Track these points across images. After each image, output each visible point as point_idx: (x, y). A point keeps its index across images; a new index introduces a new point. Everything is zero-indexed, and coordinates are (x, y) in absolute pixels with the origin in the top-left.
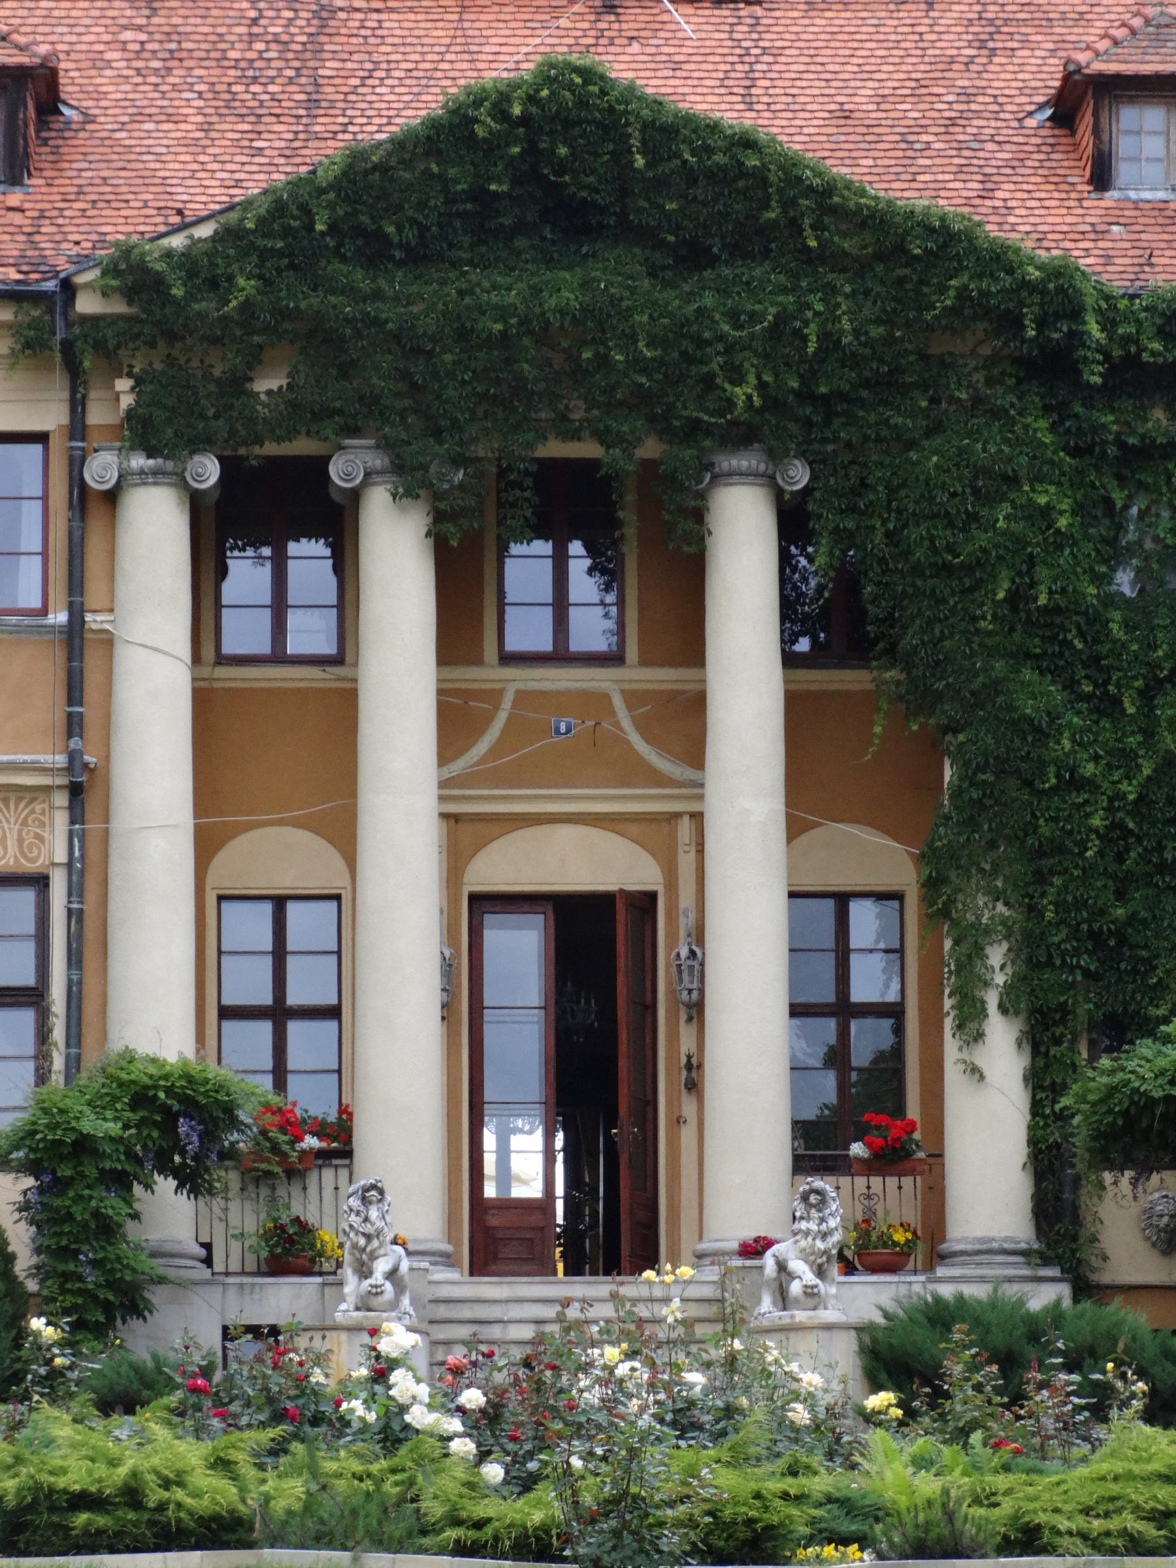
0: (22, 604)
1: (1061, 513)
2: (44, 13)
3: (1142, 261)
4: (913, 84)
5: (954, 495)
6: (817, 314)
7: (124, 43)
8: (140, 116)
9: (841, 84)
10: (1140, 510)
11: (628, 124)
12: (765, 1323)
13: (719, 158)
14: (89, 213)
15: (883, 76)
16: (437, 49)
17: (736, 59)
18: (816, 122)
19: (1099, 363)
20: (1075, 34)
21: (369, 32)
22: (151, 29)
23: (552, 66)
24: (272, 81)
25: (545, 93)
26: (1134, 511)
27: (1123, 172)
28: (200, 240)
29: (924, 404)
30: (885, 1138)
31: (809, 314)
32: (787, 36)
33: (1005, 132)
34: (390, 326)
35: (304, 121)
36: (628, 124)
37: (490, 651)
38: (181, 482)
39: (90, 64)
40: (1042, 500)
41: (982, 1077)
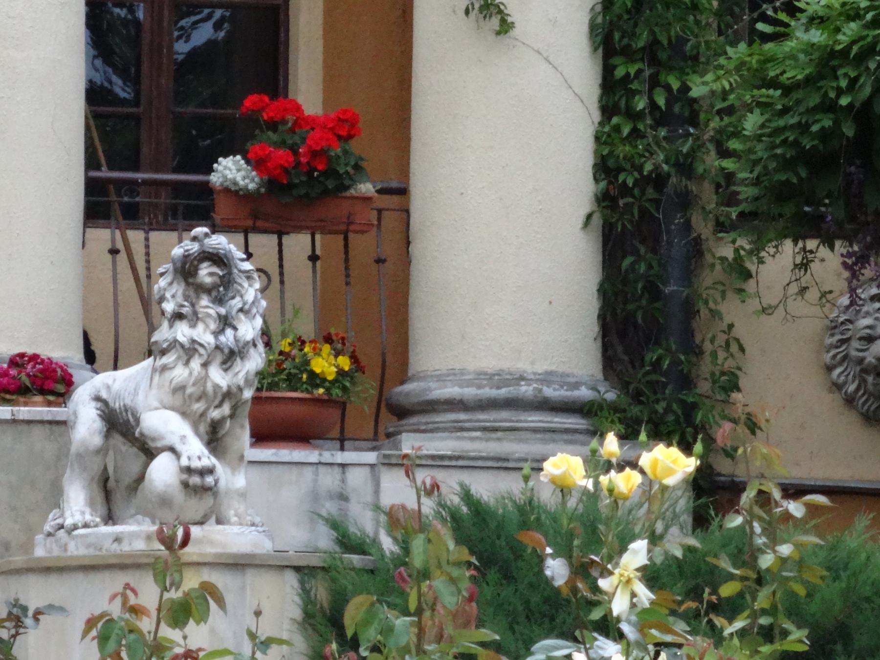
12: (76, 550)
30: (294, 149)
41: (505, 27)
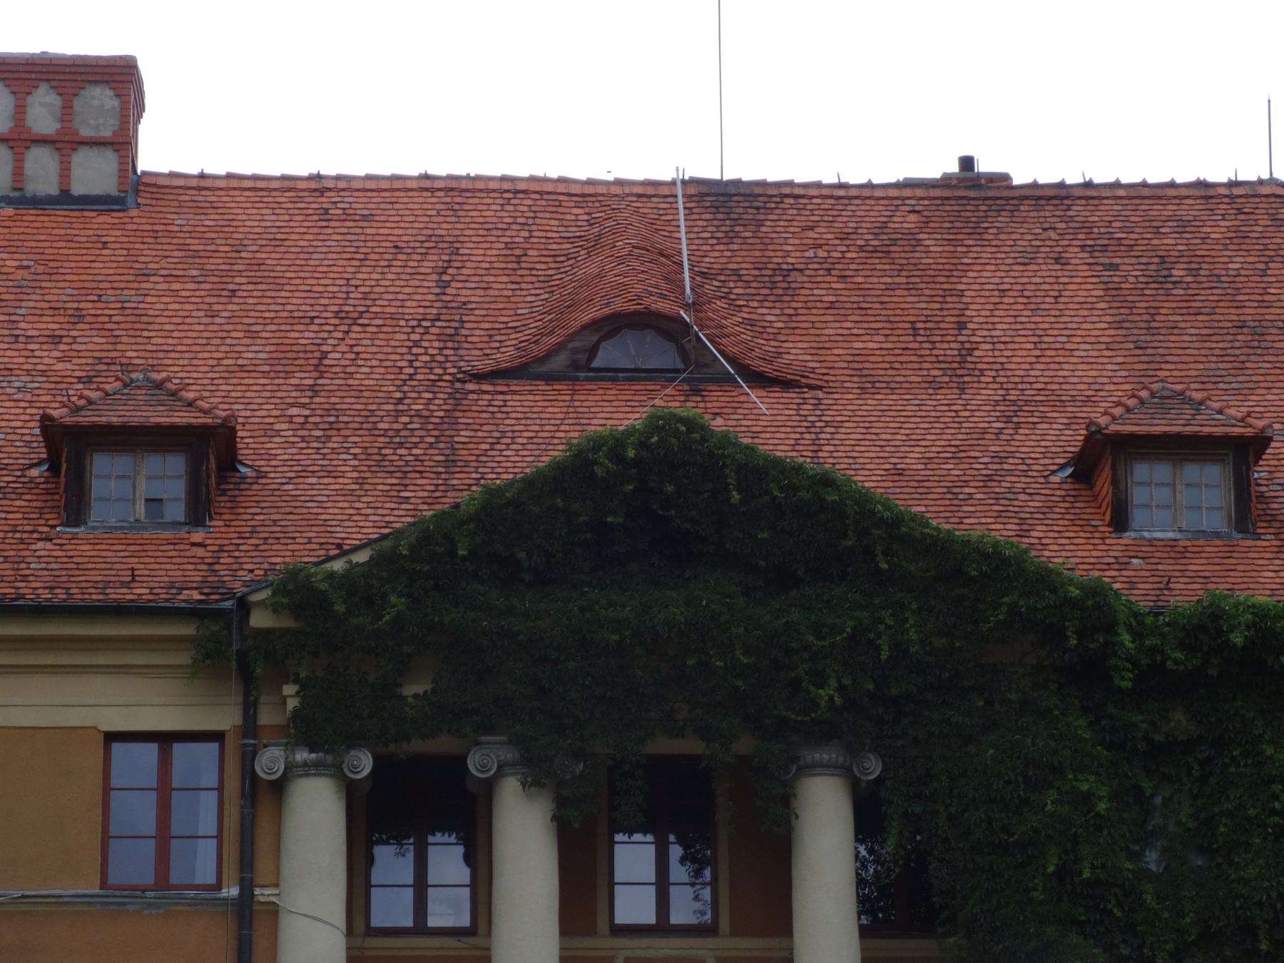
0: (199, 880)
1: (1100, 798)
2: (223, 394)
3: (1162, 586)
4: (953, 449)
5: (1008, 782)
6: (888, 627)
7: (291, 416)
8: (304, 473)
9: (893, 449)
10: (1164, 799)
11: (725, 466)
13: (803, 494)
14: (261, 548)
15: (928, 443)
16: (553, 422)
17: (804, 430)
18: (874, 478)
19: (1128, 670)
20: (1087, 412)
21: (496, 409)
22: (313, 406)
23: (660, 418)
24: (416, 445)
25: (655, 439)
26: (1158, 800)
27: (1138, 517)
28: (358, 564)
29: (981, 704)
31: (882, 627)
32: (845, 413)
33: (1034, 486)
34: (521, 637)
35: (443, 476)
36: (725, 466)
37: (603, 926)
38: (337, 773)
39: (262, 433)
40: (1085, 787)
